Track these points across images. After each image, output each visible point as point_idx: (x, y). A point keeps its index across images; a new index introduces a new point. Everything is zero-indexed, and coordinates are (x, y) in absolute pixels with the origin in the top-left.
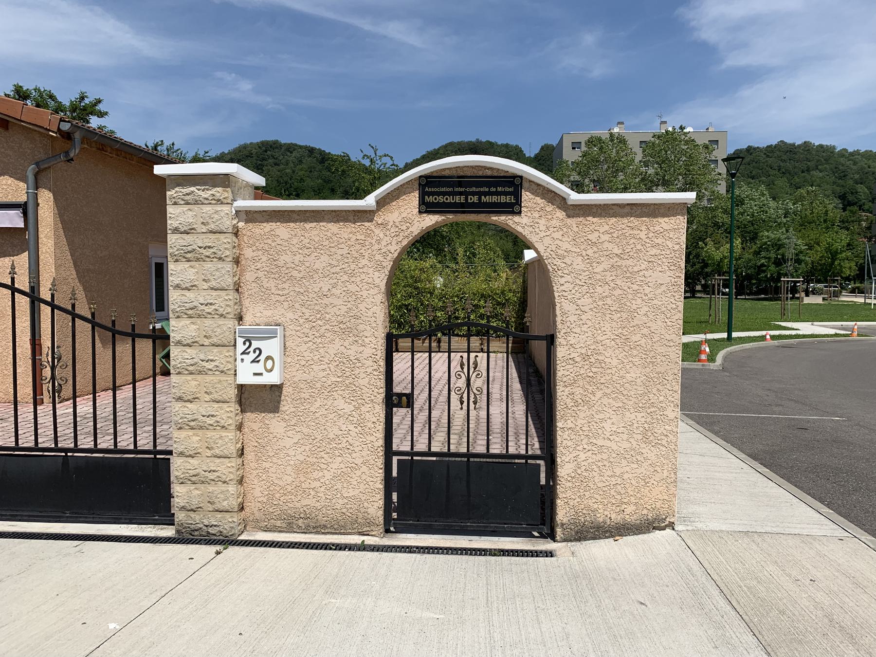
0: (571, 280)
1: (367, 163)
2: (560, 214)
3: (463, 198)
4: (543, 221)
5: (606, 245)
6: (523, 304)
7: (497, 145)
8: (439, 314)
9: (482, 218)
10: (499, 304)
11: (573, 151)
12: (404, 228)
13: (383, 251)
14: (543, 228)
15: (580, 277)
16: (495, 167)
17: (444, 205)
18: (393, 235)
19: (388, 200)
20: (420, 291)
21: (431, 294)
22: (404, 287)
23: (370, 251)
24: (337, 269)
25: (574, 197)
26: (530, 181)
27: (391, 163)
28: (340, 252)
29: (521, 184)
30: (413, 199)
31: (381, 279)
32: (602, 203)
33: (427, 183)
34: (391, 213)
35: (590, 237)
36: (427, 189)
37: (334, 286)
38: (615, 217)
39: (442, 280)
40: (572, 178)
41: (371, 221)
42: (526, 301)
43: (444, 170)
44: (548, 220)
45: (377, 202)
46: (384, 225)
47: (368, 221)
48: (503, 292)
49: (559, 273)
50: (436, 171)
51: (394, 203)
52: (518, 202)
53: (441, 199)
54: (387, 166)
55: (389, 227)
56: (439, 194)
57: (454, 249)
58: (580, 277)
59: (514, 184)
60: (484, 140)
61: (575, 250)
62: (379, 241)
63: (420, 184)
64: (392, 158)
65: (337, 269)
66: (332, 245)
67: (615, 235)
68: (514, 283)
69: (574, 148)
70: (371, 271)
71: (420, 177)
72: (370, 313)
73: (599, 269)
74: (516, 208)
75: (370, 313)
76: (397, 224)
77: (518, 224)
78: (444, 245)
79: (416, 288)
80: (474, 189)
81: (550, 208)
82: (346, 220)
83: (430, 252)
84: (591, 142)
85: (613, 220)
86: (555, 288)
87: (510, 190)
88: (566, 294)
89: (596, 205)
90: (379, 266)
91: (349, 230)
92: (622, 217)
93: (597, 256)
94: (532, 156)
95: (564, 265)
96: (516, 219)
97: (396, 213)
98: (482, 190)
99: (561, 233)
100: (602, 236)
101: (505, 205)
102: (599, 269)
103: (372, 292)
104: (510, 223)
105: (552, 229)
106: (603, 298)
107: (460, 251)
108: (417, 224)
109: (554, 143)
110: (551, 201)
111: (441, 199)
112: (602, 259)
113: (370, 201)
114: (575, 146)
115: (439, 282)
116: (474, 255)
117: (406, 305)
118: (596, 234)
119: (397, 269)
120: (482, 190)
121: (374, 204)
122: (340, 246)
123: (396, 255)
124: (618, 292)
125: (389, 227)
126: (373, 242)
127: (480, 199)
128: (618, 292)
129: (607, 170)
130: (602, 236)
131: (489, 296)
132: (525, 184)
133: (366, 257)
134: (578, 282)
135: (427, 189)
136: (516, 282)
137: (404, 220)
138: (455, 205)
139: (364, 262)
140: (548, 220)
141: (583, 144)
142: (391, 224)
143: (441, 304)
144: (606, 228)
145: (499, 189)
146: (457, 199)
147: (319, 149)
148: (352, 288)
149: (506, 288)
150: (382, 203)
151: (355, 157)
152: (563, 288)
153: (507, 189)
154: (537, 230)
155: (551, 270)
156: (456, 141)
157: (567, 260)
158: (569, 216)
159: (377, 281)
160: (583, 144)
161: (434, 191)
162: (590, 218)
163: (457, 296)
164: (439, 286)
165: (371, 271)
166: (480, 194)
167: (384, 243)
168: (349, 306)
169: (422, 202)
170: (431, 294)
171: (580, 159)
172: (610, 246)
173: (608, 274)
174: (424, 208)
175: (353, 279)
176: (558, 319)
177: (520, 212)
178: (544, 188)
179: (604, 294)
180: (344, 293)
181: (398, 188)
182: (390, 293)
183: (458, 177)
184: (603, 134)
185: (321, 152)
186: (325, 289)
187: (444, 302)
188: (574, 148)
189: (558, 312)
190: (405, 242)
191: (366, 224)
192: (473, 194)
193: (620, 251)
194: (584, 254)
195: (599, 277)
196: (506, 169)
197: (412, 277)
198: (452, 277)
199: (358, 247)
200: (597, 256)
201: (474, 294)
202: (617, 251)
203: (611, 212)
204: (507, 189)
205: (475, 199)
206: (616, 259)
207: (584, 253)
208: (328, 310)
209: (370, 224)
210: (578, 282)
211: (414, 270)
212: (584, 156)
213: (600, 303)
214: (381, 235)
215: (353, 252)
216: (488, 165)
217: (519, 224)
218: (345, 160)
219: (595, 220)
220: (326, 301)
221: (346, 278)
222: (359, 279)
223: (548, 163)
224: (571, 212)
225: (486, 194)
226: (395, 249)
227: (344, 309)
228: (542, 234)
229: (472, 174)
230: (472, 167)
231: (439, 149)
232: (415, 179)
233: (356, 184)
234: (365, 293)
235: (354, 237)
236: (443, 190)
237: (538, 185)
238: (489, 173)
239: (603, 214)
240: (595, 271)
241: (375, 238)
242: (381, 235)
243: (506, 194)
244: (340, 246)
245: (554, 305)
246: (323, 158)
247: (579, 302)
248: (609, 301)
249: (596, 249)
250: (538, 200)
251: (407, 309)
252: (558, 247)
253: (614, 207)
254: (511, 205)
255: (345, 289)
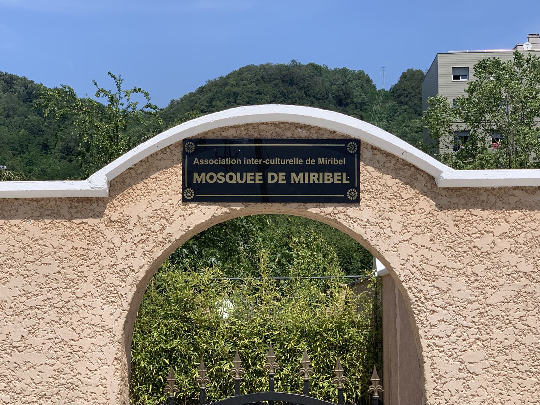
0: (448, 317)
1: (105, 101)
2: (426, 204)
3: (258, 176)
4: (397, 216)
5: (506, 257)
6: (375, 353)
7: (328, 71)
8: (226, 366)
9: (292, 209)
10: (332, 347)
11: (457, 83)
12: (156, 227)
13: (119, 268)
14: (398, 227)
15: (465, 312)
16: (312, 124)
17: (226, 188)
18: (137, 239)
19: (128, 180)
20: (193, 327)
21: (213, 330)
22: (165, 318)
23: (96, 268)
24: (38, 301)
25: (449, 175)
26: (374, 148)
27: (146, 102)
28: (44, 270)
29: (358, 153)
30: (173, 178)
31: (114, 318)
32: (496, 185)
33: (198, 154)
34: (135, 201)
35: (478, 243)
36: (196, 161)
37: (32, 330)
38: (520, 209)
39: (231, 306)
40: (454, 128)
41: (99, 215)
42: (381, 342)
43: (226, 128)
44: (407, 214)
45: (111, 184)
46: (121, 223)
47: (94, 217)
48: (339, 327)
49: (428, 304)
50: (213, 132)
51: (139, 186)
52: (354, 183)
53: (221, 178)
54: (138, 108)
55: (130, 226)
56: (216, 169)
57: (253, 251)
58: (465, 312)
59: (346, 153)
60: (305, 62)
61: (454, 265)
62: (112, 251)
63: (184, 153)
64: (146, 94)
65: (38, 301)
66: (31, 258)
67: (521, 240)
68: (358, 310)
69: (456, 77)
70: (97, 303)
71: (185, 141)
72: (95, 379)
73: (496, 299)
74: (351, 194)
75: (95, 379)
76: (145, 221)
77: (354, 220)
78: (236, 242)
79: (186, 320)
80: (277, 161)
81: (408, 193)
82: (55, 215)
83: (212, 255)
84: (483, 67)
85: (516, 214)
86: (421, 332)
87: (341, 162)
88: (440, 342)
89: (486, 189)
90: (112, 296)
91: (60, 233)
92: (532, 209)
93: (491, 275)
94: (388, 89)
95: (435, 291)
96: (352, 211)
97: (143, 203)
98: (291, 162)
99: (429, 235)
100: (498, 241)
101: (332, 188)
102: (496, 299)
103: (100, 340)
104: (341, 218)
105: (412, 230)
106: (504, 350)
107: (264, 255)
108: (179, 221)
109: (425, 68)
110: (410, 182)
111: (221, 178)
112: (501, 281)
113: (98, 181)
114: (459, 73)
115: (226, 309)
116: (289, 259)
117: (167, 351)
118: (489, 238)
119: (151, 288)
120: (291, 162)
121: (106, 186)
122: (44, 260)
123: (142, 274)
124: (530, 339)
125: (130, 226)
126: (103, 252)
127: (288, 178)
128: (530, 339)
129: (514, 113)
130: (498, 241)
131: (316, 334)
132: (365, 153)
133: (90, 278)
134: (461, 320)
135: (196, 161)
136: (363, 309)
137: (158, 214)
138: (246, 188)
139: (86, 287)
140: (407, 214)
141: (472, 72)
142: (134, 220)
143: (229, 348)
144: (505, 227)
145: (322, 161)
146: (250, 178)
147: (24, 79)
148: (65, 333)
149: (346, 320)
150: (118, 185)
151: (83, 91)
152: (434, 331)
153: (335, 161)
154: (387, 231)
155: (414, 299)
156: (257, 64)
157: (441, 283)
158: (441, 207)
159: (109, 321)
160: (472, 72)
161: (206, 166)
162: (477, 211)
163: (259, 334)
164: (226, 316)
165: (97, 303)
166: (288, 170)
167: (121, 254)
168: (58, 365)
169: (188, 183)
170: (213, 330)
171: (467, 95)
172: (513, 259)
173: (512, 306)
174: (191, 193)
175: (66, 318)
176: (429, 386)
177: (357, 201)
178: (397, 159)
179: (506, 343)
180: (49, 344)
181: (145, 161)
182: (131, 345)
183: (250, 141)
184: (504, 53)
185: (26, 83)
186: (16, 337)
187: (235, 345)
188: (456, 77)
189: (428, 374)
190: (158, 253)
191: (91, 221)
192: (277, 169)
193: (531, 268)
194: (469, 272)
195: (496, 312)
196: (332, 128)
197: (178, 301)
198: (249, 300)
199: (76, 261)
200: (491, 275)
201: (289, 331)
202: (524, 267)
203: (512, 200)
204: (335, 161)
205: (280, 178)
206: (524, 281)
207: (469, 272)
208: (19, 374)
209: (96, 221)
210: (461, 320)
211: (182, 289)
212: (471, 91)
213: (501, 358)
214: (117, 241)
215: (68, 270)
216: (301, 122)
217: (358, 220)
218: (67, 95)
219: (486, 214)
220: (17, 357)
221: (53, 315)
222: (76, 317)
223: (415, 100)
224: (444, 201)
225: (298, 169)
226: (141, 265)
227: (49, 371)
228: (397, 238)
229: (274, 136)
230: (274, 124)
231: (228, 77)
232: (176, 145)
233: (85, 139)
234: (86, 343)
235: (70, 245)
236: (223, 162)
237: (388, 155)
238: (303, 134)
239: (499, 204)
240: (489, 301)
241: (106, 245)
242: (117, 241)
243: (332, 169)
244: (44, 260)
245: (420, 363)
246: (30, 94)
247: (464, 356)
248: (515, 355)
249: (489, 264)
250: (388, 179)
251: (169, 358)
252: (424, 260)
253: (516, 192)
254: (342, 188)
255: (51, 335)
